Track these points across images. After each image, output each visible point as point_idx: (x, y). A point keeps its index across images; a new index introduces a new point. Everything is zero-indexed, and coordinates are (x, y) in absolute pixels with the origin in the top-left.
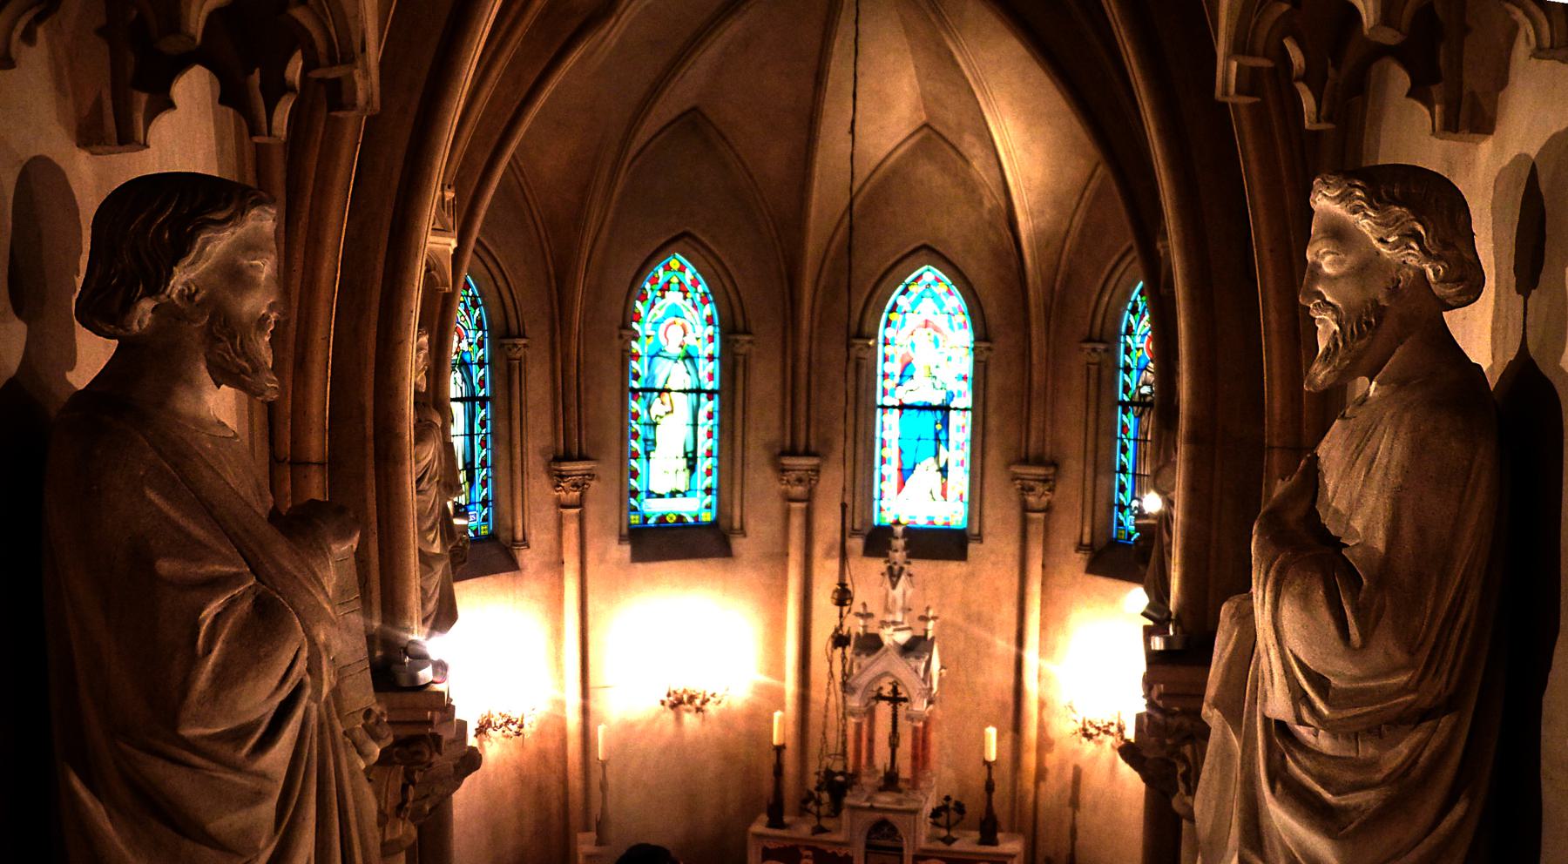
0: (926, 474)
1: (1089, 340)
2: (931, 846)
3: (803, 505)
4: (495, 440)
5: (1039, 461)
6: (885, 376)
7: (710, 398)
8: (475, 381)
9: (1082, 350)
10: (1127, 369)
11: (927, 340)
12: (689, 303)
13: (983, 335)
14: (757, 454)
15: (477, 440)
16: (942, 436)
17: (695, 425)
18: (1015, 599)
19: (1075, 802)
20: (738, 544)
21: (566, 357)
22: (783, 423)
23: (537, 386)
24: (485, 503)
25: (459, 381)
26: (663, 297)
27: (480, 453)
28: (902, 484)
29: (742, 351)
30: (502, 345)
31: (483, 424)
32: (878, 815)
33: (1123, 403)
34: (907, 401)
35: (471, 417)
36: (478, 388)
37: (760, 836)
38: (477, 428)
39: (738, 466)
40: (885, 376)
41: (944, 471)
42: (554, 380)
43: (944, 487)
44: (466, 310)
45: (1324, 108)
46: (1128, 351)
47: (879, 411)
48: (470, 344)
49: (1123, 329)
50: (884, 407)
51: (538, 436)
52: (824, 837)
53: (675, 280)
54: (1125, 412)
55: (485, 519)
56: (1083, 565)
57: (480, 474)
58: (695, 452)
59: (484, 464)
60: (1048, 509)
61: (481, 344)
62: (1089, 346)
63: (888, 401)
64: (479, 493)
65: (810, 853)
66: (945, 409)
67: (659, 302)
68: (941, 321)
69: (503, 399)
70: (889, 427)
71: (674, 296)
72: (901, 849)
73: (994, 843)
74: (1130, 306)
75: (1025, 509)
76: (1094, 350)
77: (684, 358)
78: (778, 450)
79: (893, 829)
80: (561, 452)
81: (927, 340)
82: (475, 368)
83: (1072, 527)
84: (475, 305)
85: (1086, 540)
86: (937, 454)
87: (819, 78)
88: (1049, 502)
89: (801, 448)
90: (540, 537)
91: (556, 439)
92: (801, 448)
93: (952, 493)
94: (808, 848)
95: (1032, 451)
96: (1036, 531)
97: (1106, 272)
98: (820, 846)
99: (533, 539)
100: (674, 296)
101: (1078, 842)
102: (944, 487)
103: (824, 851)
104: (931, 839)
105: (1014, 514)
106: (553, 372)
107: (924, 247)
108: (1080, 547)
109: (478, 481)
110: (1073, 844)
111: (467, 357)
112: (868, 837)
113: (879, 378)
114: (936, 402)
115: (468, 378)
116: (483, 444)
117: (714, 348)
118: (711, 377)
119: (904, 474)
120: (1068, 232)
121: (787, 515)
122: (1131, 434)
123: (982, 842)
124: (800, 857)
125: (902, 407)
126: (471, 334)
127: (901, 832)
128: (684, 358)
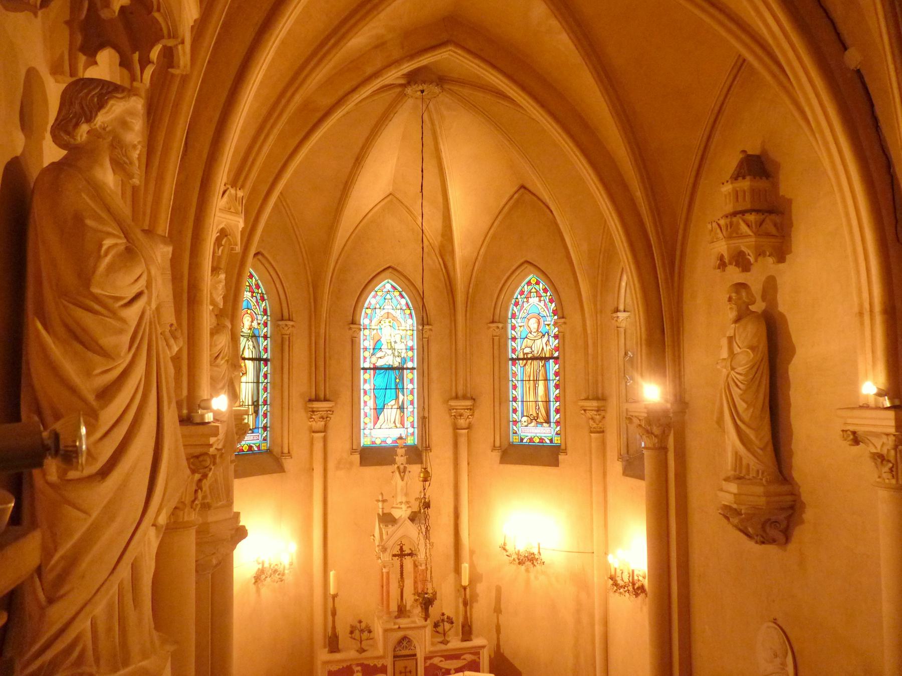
0: (391, 413)
1: (493, 322)
2: (432, 649)
3: (322, 434)
4: (273, 388)
5: (465, 398)
6: (365, 349)
7: (266, 365)
8: (261, 348)
9: (489, 328)
10: (514, 339)
11: (388, 325)
12: (254, 300)
13: (424, 321)
14: (297, 402)
15: (261, 387)
16: (400, 386)
17: (258, 382)
18: (452, 485)
19: (498, 610)
20: (288, 463)
21: (318, 335)
22: (310, 379)
23: (300, 352)
24: (265, 428)
25: (251, 347)
26: (527, 302)
27: (263, 396)
28: (377, 418)
29: (288, 332)
30: (278, 326)
31: (265, 376)
32: (401, 634)
33: (512, 359)
34: (379, 364)
35: (258, 371)
36: (263, 353)
37: (326, 663)
38: (262, 379)
39: (286, 410)
40: (365, 349)
41: (401, 408)
42: (310, 350)
43: (402, 418)
44: (257, 302)
45: (63, 114)
46: (514, 328)
47: (362, 371)
48: (259, 324)
49: (510, 315)
50: (364, 369)
51: (300, 385)
52: (364, 655)
53: (534, 290)
54: (514, 364)
55: (265, 440)
56: (498, 459)
57: (262, 409)
58: (258, 401)
59: (265, 403)
60: (469, 427)
61: (265, 325)
62: (495, 325)
63: (367, 365)
64: (262, 422)
65: (359, 668)
66: (401, 369)
67: (526, 305)
68: (398, 314)
69: (278, 360)
70: (367, 382)
71: (534, 300)
72: (415, 655)
73: (469, 640)
74: (513, 301)
75: (456, 428)
76: (498, 327)
77: (252, 337)
78: (307, 399)
79: (410, 641)
80: (313, 397)
81: (388, 325)
82: (261, 340)
83: (484, 437)
84: (263, 299)
85: (498, 444)
86: (397, 397)
87: (359, 160)
88: (470, 423)
89: (322, 396)
90: (299, 451)
91: (311, 387)
92: (322, 396)
93: (407, 424)
94: (358, 665)
95: (460, 393)
96: (463, 441)
97: (502, 282)
98: (366, 662)
99: (294, 453)
100: (534, 300)
101: (502, 636)
102: (402, 418)
103: (369, 665)
104: (433, 644)
105: (449, 431)
106: (310, 344)
107: (389, 267)
108: (494, 448)
109: (261, 413)
110: (498, 639)
111: (257, 333)
112: (394, 650)
113: (415, 347)
114: (396, 365)
115: (256, 346)
116: (265, 389)
117: (267, 330)
118: (266, 350)
119: (378, 411)
120: (477, 258)
121: (312, 444)
122: (519, 377)
123: (463, 640)
124: (353, 672)
125: (375, 368)
126: (260, 317)
127: (415, 642)
128: (252, 337)
